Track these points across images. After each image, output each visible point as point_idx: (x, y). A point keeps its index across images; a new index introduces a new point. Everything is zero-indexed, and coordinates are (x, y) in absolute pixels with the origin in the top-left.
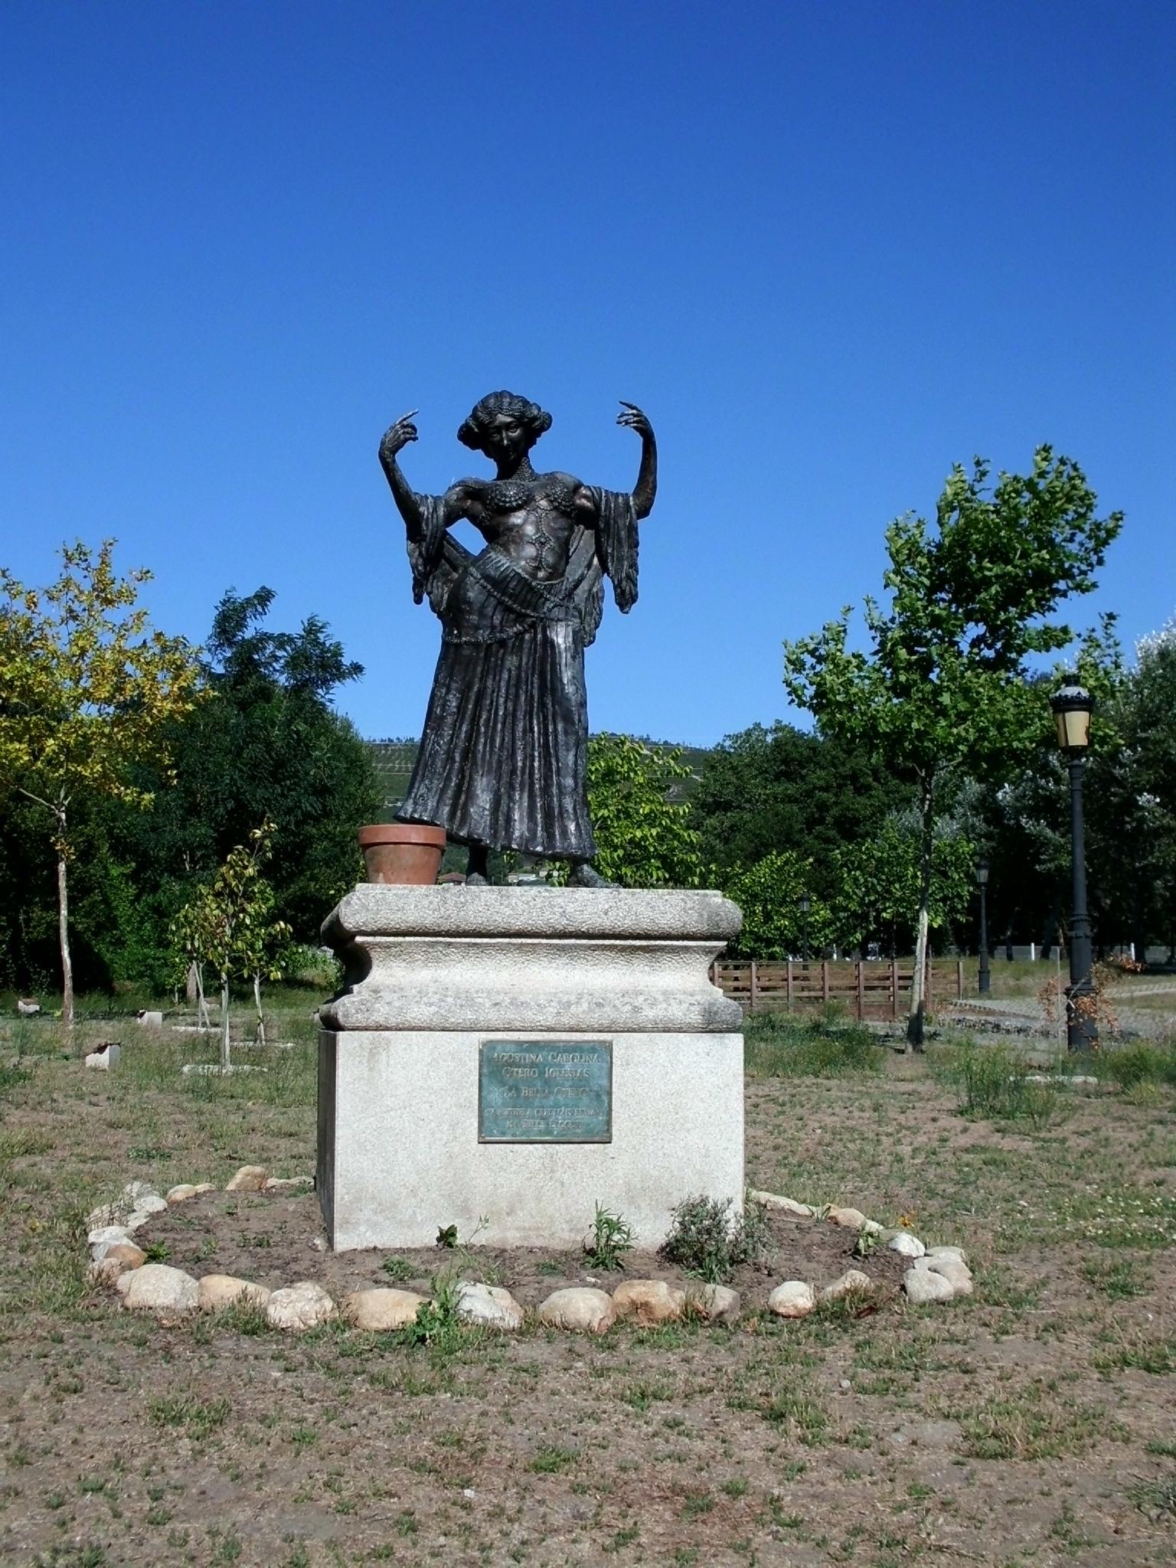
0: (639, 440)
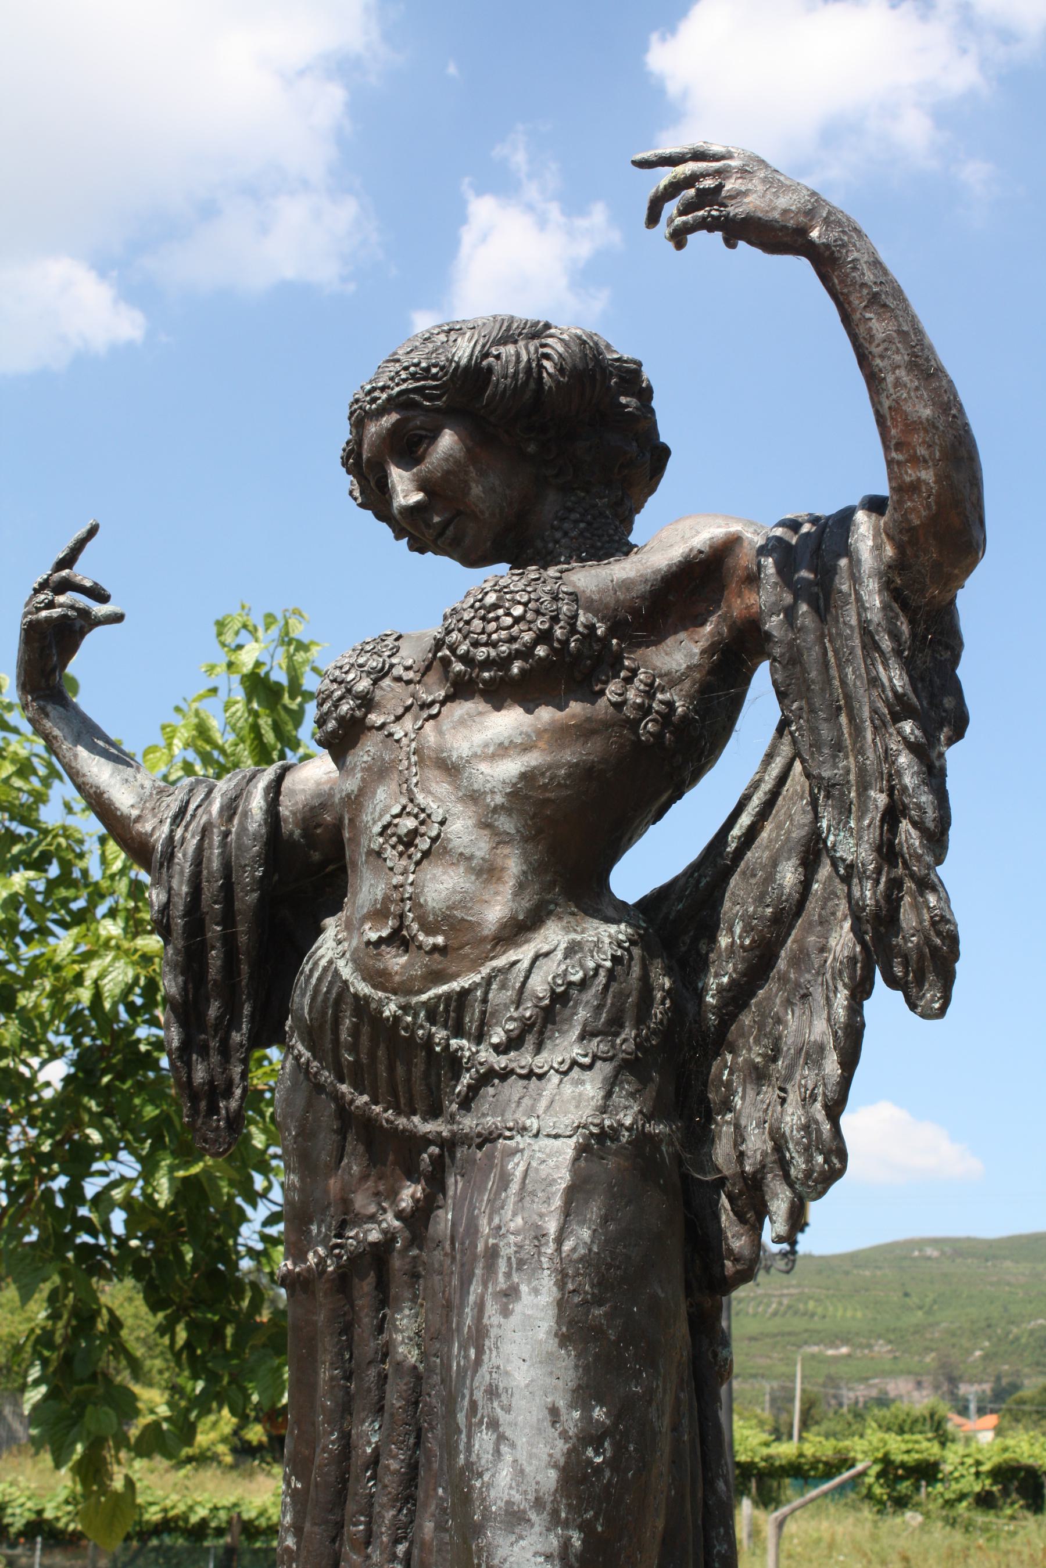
0: (801, 267)
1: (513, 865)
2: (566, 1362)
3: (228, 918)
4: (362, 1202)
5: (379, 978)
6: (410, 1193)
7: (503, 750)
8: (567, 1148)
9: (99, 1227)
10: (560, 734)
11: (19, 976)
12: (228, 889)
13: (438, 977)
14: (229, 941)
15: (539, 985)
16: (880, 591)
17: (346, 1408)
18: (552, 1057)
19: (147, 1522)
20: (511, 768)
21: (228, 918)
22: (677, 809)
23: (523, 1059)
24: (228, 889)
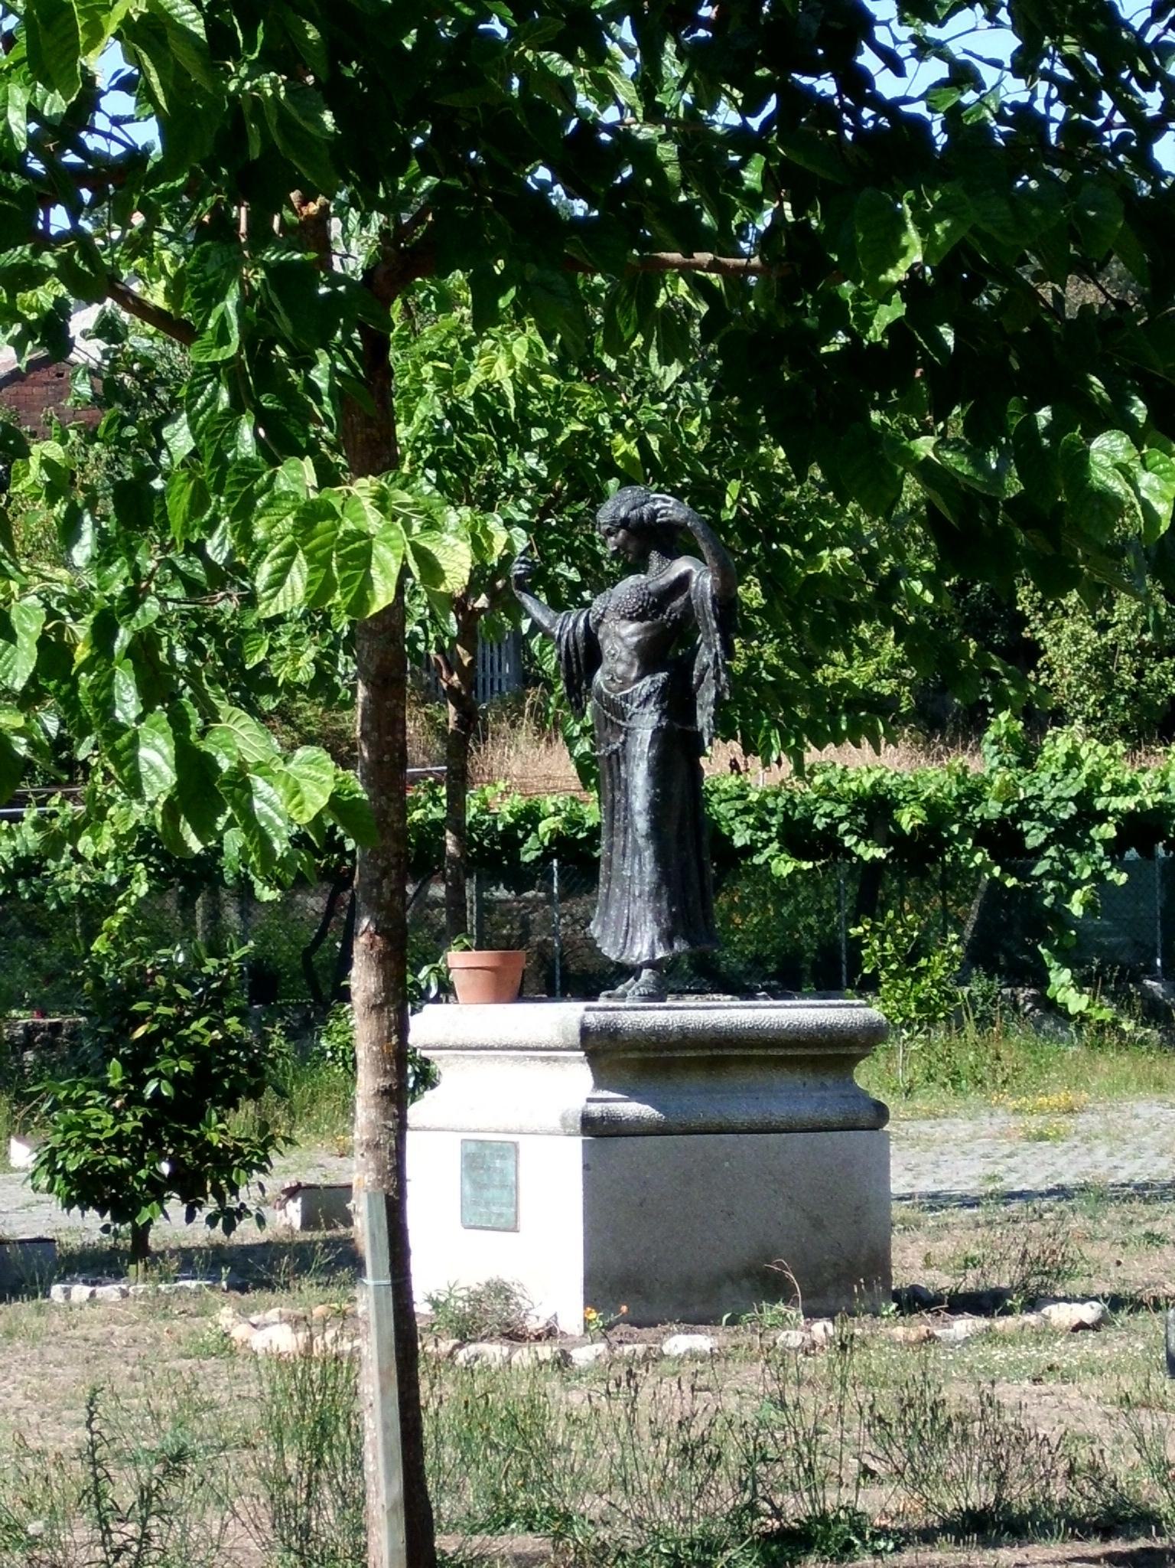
1: (637, 663)
2: (650, 780)
3: (577, 656)
4: (611, 739)
5: (609, 689)
6: (622, 737)
7: (633, 635)
8: (650, 732)
9: (496, 213)
10: (647, 629)
11: (473, 283)
12: (576, 650)
13: (621, 690)
14: (578, 662)
15: (644, 693)
16: (656, 894)
17: (612, 790)
18: (647, 710)
19: (591, 943)
20: (635, 639)
21: (577, 656)
22: (582, 1296)
23: (641, 709)
24: (576, 650)
